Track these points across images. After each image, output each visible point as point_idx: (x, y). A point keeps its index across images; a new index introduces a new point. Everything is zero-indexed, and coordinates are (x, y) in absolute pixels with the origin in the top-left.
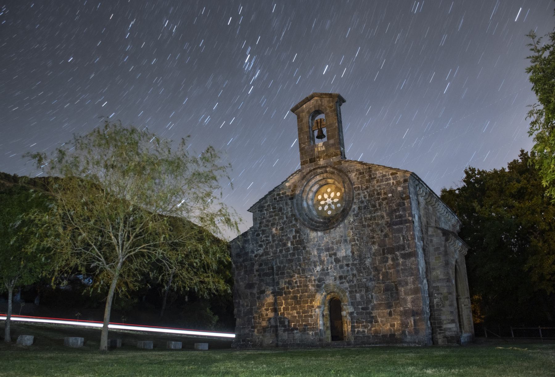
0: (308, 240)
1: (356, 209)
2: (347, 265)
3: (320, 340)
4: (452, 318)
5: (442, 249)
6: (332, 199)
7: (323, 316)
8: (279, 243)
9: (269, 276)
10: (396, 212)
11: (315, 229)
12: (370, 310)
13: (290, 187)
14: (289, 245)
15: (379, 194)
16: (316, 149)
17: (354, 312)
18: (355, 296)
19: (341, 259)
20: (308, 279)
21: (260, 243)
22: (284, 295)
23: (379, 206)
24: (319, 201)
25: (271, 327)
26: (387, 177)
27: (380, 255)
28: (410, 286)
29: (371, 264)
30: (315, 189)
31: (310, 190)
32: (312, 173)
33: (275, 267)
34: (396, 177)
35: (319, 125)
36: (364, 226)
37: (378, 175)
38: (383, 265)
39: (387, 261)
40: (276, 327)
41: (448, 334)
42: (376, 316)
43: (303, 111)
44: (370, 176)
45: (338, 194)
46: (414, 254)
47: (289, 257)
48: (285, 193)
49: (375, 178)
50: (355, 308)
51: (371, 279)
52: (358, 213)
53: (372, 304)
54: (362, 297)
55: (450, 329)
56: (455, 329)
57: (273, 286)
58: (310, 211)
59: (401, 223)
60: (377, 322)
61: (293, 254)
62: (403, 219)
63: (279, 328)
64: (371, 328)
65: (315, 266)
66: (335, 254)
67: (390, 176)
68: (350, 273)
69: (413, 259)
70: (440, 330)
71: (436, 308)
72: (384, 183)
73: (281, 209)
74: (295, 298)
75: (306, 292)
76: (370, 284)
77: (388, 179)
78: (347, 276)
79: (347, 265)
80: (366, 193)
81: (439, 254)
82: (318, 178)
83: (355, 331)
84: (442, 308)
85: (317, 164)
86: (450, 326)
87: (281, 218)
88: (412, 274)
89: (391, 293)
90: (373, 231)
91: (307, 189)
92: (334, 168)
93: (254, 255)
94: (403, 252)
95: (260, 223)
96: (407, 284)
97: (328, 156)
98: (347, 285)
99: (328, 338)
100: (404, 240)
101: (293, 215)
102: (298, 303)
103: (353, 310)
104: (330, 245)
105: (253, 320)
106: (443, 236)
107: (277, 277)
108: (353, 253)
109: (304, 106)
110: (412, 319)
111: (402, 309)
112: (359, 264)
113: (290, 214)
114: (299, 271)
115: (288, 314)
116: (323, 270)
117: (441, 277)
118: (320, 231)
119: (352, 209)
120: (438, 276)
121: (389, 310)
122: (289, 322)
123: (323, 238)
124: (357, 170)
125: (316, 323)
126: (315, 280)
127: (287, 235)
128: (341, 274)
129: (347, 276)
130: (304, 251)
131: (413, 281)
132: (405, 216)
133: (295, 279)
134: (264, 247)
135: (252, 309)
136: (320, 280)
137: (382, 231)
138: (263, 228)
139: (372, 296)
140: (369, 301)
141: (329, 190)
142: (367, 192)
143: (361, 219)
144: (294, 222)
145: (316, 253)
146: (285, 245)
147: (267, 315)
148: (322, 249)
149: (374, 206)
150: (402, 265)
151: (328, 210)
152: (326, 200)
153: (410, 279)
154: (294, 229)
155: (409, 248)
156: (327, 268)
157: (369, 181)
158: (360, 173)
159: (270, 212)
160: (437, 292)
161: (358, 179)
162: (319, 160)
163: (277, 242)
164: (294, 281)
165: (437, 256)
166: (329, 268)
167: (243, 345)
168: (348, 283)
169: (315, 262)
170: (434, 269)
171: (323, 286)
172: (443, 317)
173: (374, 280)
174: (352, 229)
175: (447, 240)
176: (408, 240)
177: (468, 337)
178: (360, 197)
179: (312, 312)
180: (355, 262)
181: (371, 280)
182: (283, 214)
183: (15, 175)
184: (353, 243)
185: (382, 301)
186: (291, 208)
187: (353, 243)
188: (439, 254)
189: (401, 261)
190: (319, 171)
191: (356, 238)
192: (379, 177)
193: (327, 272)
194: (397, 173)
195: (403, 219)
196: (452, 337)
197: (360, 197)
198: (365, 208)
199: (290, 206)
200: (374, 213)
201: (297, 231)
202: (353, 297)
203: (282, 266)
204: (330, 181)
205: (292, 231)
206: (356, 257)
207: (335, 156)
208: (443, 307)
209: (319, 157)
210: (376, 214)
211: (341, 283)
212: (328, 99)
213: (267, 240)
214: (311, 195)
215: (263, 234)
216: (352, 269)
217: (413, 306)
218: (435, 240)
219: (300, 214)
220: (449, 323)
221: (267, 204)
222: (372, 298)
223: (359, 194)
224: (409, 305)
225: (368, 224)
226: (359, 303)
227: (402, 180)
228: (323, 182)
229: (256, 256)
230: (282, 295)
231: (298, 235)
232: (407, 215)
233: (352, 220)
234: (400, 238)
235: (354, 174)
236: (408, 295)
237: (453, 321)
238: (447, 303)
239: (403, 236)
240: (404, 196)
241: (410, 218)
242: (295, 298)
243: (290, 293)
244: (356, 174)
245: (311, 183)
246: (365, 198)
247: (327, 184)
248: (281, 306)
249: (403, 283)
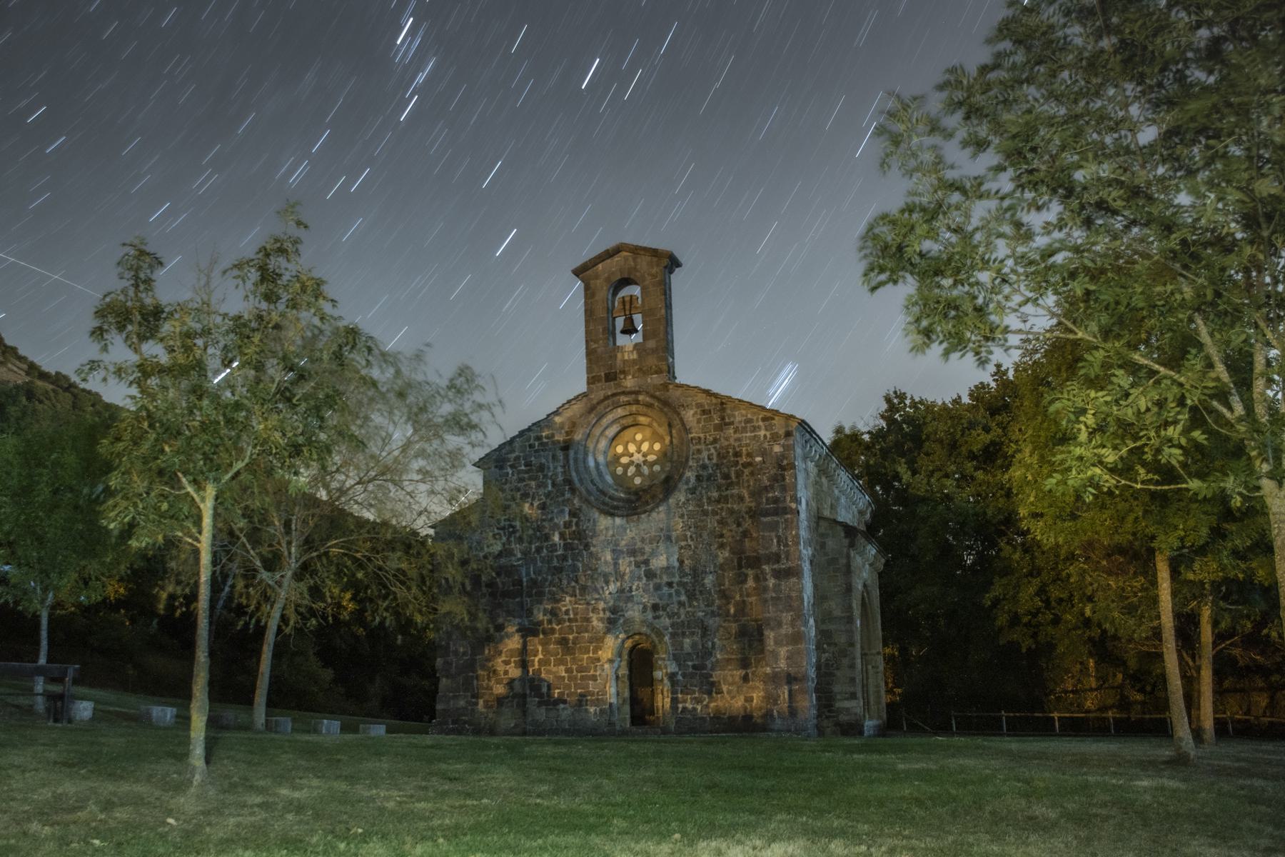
1: (693, 480)
2: (670, 585)
10: (768, 492)
28: (786, 630)
32: (610, 401)
34: (771, 426)
44: (723, 419)
45: (657, 447)
49: (732, 423)
55: (848, 709)
66: (646, 562)
67: (761, 423)
68: (675, 599)
76: (711, 622)
79: (670, 585)
80: (713, 451)
82: (620, 412)
85: (619, 385)
87: (544, 485)
91: (597, 431)
96: (780, 625)
104: (639, 545)
108: (681, 562)
124: (699, 405)
139: (713, 644)
140: (708, 653)
146: (547, 538)
147: (506, 672)
149: (726, 477)
158: (704, 412)
184: (683, 543)
187: (683, 543)
191: (689, 534)
204: (642, 419)
205: (562, 511)
206: (687, 571)
207: (656, 373)
216: (678, 593)
220: (847, 699)
221: (513, 455)
223: (699, 451)
224: (783, 664)
235: (692, 412)
236: (782, 645)
239: (779, 538)
244: (696, 413)
245: (605, 421)
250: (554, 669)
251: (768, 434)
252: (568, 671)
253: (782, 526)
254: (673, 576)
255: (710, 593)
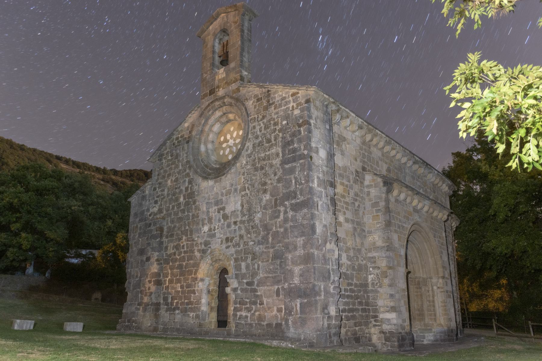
0: (198, 191)
1: (251, 147)
2: (235, 223)
3: (200, 325)
4: (392, 304)
5: (382, 204)
6: (234, 140)
7: (209, 292)
8: (172, 198)
9: (156, 239)
10: (289, 145)
11: (206, 178)
12: (255, 287)
13: (188, 127)
14: (182, 199)
15: (276, 124)
16: (217, 77)
17: (237, 288)
18: (240, 265)
19: (229, 215)
20: (195, 243)
21: (156, 199)
22: (171, 264)
23: (275, 140)
24: (221, 143)
25: (151, 305)
26: (287, 100)
27: (272, 208)
28: (300, 252)
29: (260, 221)
30: (216, 128)
31: (210, 130)
32: (210, 107)
33: (165, 228)
34: (297, 98)
35: (225, 48)
36: (256, 169)
37: (277, 99)
38: (273, 222)
39: (278, 217)
40: (158, 304)
41: (386, 327)
42: (261, 295)
43: (209, 35)
44: (268, 101)
45: (241, 133)
46: (307, 204)
47: (180, 215)
48: (184, 135)
49: (273, 103)
50: (239, 283)
51: (259, 241)
52: (252, 153)
53: (258, 278)
54: (247, 267)
55: (389, 320)
56: (395, 321)
57: (159, 251)
58: (208, 156)
59: (294, 160)
60: (262, 303)
61: (183, 211)
62: (298, 153)
63: (162, 306)
64: (255, 312)
65: (203, 225)
66: (223, 209)
67: (291, 98)
68: (238, 233)
69: (305, 210)
70: (375, 321)
71: (370, 288)
72: (283, 108)
73: (177, 156)
74: (180, 267)
75: (192, 259)
76: (257, 249)
77: (287, 103)
78: (233, 238)
79: (235, 223)
80: (262, 125)
81: (378, 211)
82: (218, 114)
83: (237, 315)
84: (379, 289)
85: (216, 96)
86: (388, 316)
87: (177, 167)
88: (303, 234)
89: (281, 262)
90: (265, 175)
91: (207, 129)
92: (232, 98)
93: (149, 214)
94: (293, 202)
95: (158, 175)
96: (295, 248)
97: (228, 84)
98: (232, 250)
99: (211, 322)
100: (296, 184)
101: (188, 162)
102: (182, 274)
103: (237, 286)
104: (220, 197)
105: (140, 295)
106: (384, 186)
107: (166, 240)
108: (242, 206)
109: (211, 27)
110: (298, 301)
111: (286, 286)
112: (248, 221)
113: (185, 161)
114: (187, 233)
115: (173, 288)
116: (210, 230)
117: (380, 243)
118: (211, 179)
119: (246, 148)
120: (374, 243)
121: (276, 287)
122: (173, 299)
123: (213, 188)
124: (256, 96)
125: (199, 302)
126: (201, 244)
127: (180, 187)
128: (228, 235)
129: (233, 238)
130: (193, 206)
131: (303, 244)
132: (300, 149)
133: (182, 243)
134: (159, 203)
135: (140, 280)
136: (207, 244)
137: (275, 174)
138: (160, 181)
139: (259, 265)
140: (254, 274)
141: (232, 129)
142: (263, 123)
143: (254, 160)
144: (188, 171)
145: (205, 209)
146: (177, 199)
147: (149, 288)
148: (211, 203)
149: (269, 141)
150: (292, 221)
151: (229, 154)
152: (228, 141)
153: (300, 241)
154: (187, 179)
155: (301, 195)
156: (215, 227)
157: (266, 108)
158: (258, 100)
159: (169, 160)
160: (373, 265)
161: (255, 107)
162: (219, 91)
163: (170, 197)
164: (182, 245)
165: (375, 214)
166: (217, 227)
167: (127, 326)
168: (234, 247)
169: (203, 220)
170: (370, 232)
171: (209, 251)
172: (380, 303)
173: (262, 244)
174: (243, 174)
175: (389, 191)
176: (301, 184)
177: (441, 332)
178: (255, 130)
179: (195, 287)
180: (244, 219)
181: (259, 243)
182: (179, 161)
183: (104, 167)
184: (243, 193)
185: (269, 273)
186: (187, 153)
187: (243, 193)
188: (378, 211)
189: (291, 214)
190: (217, 103)
191: (247, 185)
192: (278, 101)
193: (213, 232)
194: (298, 93)
195: (298, 153)
196: (391, 333)
197: (255, 130)
198: (259, 145)
199: (186, 152)
200: (269, 150)
201: (190, 182)
202: (238, 267)
203: (173, 226)
204: (231, 116)
205: (185, 181)
206: (245, 212)
207: (234, 82)
208: (381, 287)
209: (218, 87)
210: (270, 152)
211: (227, 247)
212: (233, 13)
213: (162, 195)
214: (211, 136)
215: (159, 188)
216: (240, 228)
217: (301, 282)
218: (374, 192)
219: (194, 160)
220: (388, 312)
221: (166, 152)
222: (258, 269)
223: (254, 127)
224: (296, 281)
225: (261, 166)
226: (244, 276)
227: (303, 101)
228: (224, 119)
229: (150, 215)
230: (169, 263)
231: (190, 186)
232: (302, 147)
233: (244, 162)
234: (291, 181)
235: (252, 102)
236: (297, 265)
237: (393, 309)
238: (386, 281)
239: (296, 178)
240: (301, 121)
241: (306, 152)
242: (180, 267)
243: (176, 260)
244: (254, 102)
245: (210, 122)
246: (260, 131)
247: (229, 121)
248: (167, 277)
249: (291, 247)
250: (175, 286)
251: (295, 105)
252: (182, 287)
253: (298, 169)
254: (238, 217)
255: (257, 227)
